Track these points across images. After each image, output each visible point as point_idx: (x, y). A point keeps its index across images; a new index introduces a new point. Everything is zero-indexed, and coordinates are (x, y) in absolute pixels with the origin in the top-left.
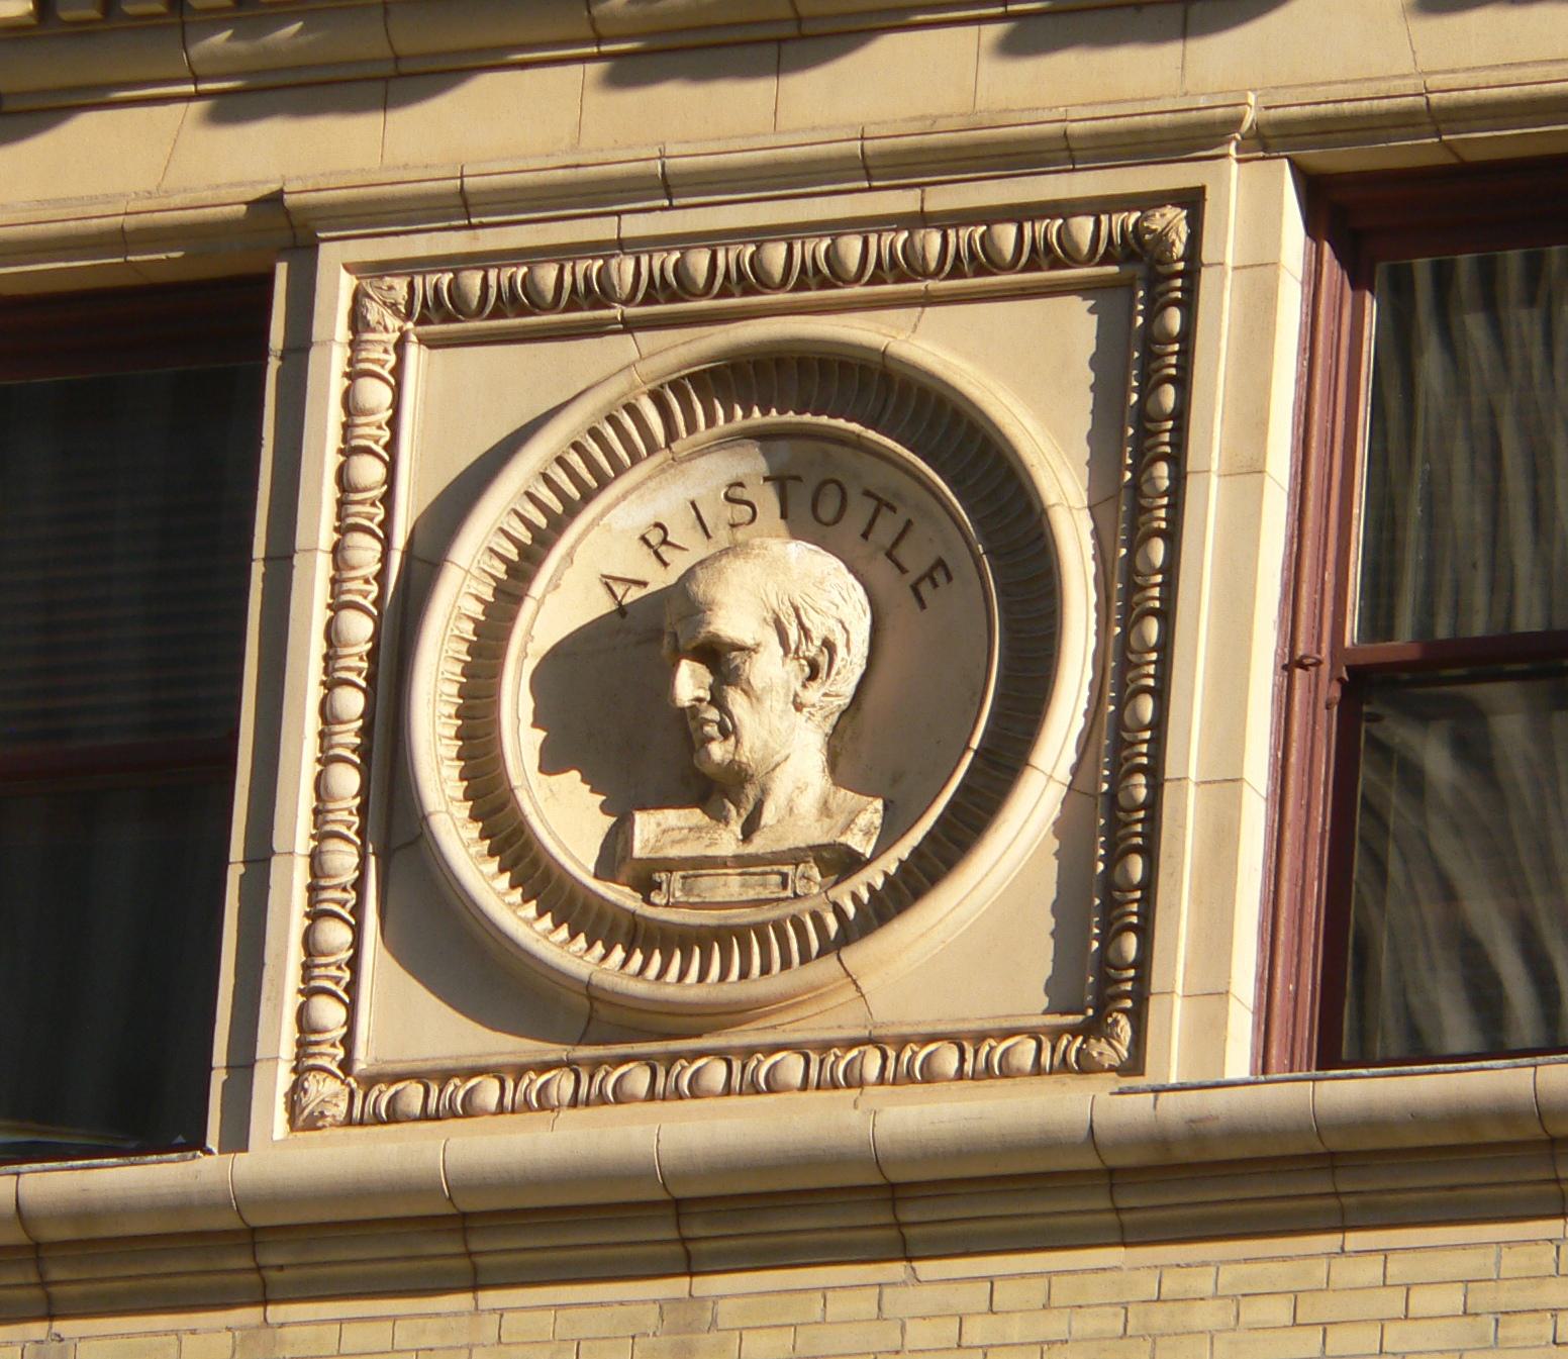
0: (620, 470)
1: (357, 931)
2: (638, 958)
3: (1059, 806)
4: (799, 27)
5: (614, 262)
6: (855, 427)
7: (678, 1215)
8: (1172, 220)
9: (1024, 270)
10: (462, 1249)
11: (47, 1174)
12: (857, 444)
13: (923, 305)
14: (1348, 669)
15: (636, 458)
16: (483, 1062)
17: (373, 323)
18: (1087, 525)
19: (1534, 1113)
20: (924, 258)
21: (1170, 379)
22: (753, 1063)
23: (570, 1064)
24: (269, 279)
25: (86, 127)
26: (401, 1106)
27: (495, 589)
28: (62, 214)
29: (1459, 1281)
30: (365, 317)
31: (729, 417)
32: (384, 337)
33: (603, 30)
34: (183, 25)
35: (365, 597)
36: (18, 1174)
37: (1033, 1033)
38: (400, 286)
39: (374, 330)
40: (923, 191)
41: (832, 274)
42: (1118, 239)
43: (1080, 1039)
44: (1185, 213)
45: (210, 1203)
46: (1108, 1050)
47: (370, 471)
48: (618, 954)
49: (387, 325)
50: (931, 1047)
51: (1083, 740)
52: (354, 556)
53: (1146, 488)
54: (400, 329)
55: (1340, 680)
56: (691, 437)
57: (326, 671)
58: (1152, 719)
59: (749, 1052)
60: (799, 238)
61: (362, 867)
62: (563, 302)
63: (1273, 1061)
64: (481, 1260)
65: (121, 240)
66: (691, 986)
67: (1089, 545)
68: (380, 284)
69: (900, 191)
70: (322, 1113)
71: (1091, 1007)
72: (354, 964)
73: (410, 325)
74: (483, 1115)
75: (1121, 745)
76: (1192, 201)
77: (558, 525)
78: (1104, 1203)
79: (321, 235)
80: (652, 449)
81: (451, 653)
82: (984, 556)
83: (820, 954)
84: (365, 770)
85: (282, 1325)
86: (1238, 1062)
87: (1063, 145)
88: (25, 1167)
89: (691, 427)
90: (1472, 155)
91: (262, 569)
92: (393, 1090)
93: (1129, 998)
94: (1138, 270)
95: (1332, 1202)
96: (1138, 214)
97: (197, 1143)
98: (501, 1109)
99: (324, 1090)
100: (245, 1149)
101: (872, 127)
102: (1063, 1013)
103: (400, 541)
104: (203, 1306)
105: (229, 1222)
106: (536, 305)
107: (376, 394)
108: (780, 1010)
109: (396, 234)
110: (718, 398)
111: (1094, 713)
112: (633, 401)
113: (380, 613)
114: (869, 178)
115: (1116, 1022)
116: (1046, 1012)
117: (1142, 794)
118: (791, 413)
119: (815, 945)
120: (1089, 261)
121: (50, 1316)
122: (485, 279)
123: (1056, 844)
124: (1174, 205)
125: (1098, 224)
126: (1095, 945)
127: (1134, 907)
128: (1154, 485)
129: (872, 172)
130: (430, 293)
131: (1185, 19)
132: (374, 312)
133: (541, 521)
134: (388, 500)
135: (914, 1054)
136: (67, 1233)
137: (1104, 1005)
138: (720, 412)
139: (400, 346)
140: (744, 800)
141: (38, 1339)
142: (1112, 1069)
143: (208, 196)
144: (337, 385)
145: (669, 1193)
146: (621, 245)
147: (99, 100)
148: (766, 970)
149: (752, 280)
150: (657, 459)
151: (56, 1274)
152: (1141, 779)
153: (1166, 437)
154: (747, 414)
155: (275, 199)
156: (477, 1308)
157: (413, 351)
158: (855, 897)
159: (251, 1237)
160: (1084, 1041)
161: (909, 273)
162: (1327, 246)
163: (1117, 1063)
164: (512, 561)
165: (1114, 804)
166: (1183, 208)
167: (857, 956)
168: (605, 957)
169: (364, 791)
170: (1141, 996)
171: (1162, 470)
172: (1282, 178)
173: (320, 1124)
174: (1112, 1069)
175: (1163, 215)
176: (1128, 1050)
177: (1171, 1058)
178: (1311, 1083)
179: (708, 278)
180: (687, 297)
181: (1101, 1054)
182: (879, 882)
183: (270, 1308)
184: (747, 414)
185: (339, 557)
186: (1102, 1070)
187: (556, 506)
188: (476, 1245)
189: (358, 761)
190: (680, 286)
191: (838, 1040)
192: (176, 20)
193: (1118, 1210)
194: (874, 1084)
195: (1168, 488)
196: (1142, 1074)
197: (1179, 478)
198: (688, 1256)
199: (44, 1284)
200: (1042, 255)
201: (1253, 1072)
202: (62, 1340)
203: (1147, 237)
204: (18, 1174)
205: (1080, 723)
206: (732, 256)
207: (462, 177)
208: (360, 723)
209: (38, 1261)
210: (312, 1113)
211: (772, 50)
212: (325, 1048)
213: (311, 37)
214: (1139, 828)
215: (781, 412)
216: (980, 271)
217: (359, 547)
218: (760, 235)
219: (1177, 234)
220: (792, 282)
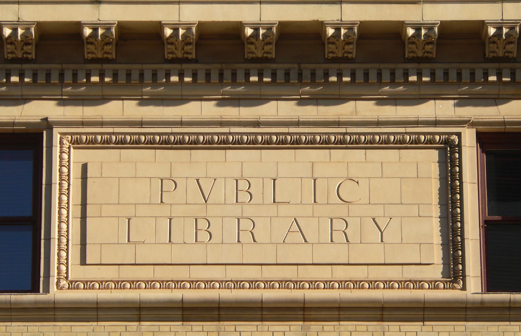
9: (102, 144)
10: (139, 313)
16: (423, 279)
17: (64, 144)
19: (382, 302)
20: (406, 140)
24: (43, 133)
29: (152, 331)
30: (63, 142)
32: (66, 146)
34: (142, 85)
37: (441, 281)
39: (65, 145)
40: (289, 129)
42: (444, 140)
44: (457, 136)
45: (44, 302)
46: (458, 286)
52: (63, 185)
54: (69, 145)
57: (59, 206)
58: (460, 226)
68: (65, 136)
70: (64, 287)
71: (452, 277)
73: (71, 145)
74: (245, 289)
76: (459, 135)
79: (54, 126)
85: (142, 325)
91: (45, 186)
93: (461, 276)
97: (38, 291)
99: (63, 283)
100: (49, 293)
101: (17, 117)
102: (446, 278)
104: (411, 321)
105: (337, 306)
106: (242, 143)
107: (65, 156)
109: (185, 127)
114: (83, 126)
115: (460, 281)
116: (442, 278)
127: (460, 260)
130: (76, 139)
132: (65, 141)
139: (69, 148)
142: (459, 289)
144: (58, 154)
147: (40, 98)
152: (459, 238)
155: (46, 119)
157: (72, 149)
163: (460, 288)
166: (457, 136)
173: (63, 289)
174: (459, 289)
175: (453, 137)
176: (462, 286)
186: (457, 289)
188: (341, 313)
198: (219, 318)
200: (414, 142)
203: (450, 140)
207: (142, 118)
209: (424, 310)
210: (62, 287)
212: (63, 274)
214: (460, 246)
218: (360, 134)
219: (456, 140)
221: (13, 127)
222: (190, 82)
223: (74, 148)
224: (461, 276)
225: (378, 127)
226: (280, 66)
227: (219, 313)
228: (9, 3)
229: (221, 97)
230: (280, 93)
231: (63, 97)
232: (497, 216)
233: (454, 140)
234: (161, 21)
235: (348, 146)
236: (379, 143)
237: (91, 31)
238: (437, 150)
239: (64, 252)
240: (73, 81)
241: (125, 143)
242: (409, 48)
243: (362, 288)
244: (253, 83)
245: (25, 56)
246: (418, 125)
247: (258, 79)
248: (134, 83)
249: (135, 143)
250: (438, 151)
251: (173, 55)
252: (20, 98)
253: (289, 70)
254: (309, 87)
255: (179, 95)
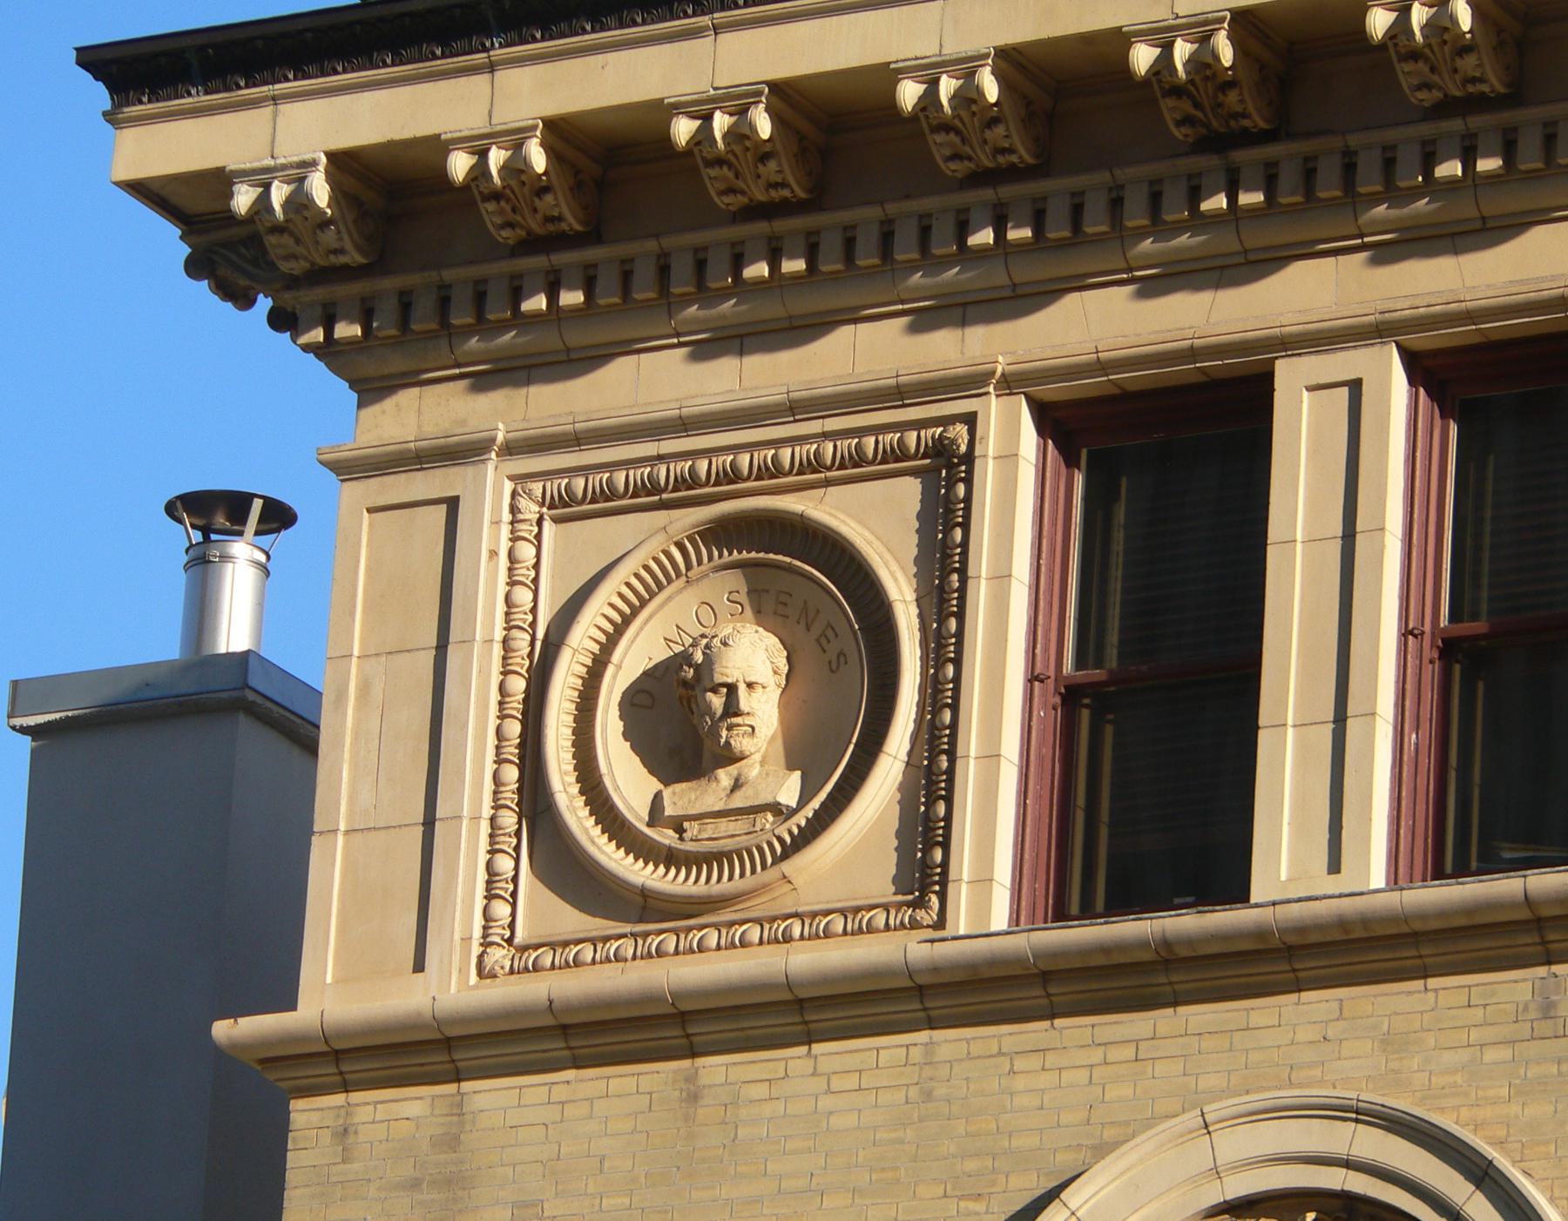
0: (660, 587)
1: (517, 860)
2: (673, 871)
3: (901, 775)
4: (568, 355)
5: (656, 468)
6: (788, 560)
7: (684, 1021)
8: (960, 431)
9: (880, 464)
11: (1544, 876)
12: (790, 569)
13: (826, 487)
14: (1065, 687)
15: (670, 581)
18: (914, 611)
21: (959, 524)
22: (776, 925)
23: (635, 935)
25: (843, 335)
26: (874, 924)
27: (593, 659)
28: (1525, 289)
31: (721, 556)
33: (1133, 264)
34: (1354, 203)
35: (522, 668)
36: (1525, 876)
37: (886, 907)
38: (537, 488)
41: (773, 470)
43: (911, 909)
44: (966, 427)
46: (927, 917)
47: (523, 596)
48: (662, 869)
49: (530, 509)
50: (745, 927)
51: (914, 737)
53: (947, 588)
54: (539, 512)
55: (1060, 694)
56: (700, 568)
59: (731, 924)
60: (550, 479)
61: (520, 823)
62: (670, 487)
63: (1023, 919)
64: (347, 1077)
65: (1192, 354)
66: (713, 885)
67: (916, 622)
69: (894, 410)
71: (917, 891)
72: (515, 879)
73: (545, 510)
74: (665, 956)
75: (933, 739)
76: (970, 420)
77: (627, 621)
78: (333, 1070)
80: (678, 575)
81: (568, 697)
82: (858, 632)
83: (772, 864)
84: (521, 768)
86: (1000, 919)
87: (896, 391)
88: (1529, 872)
89: (700, 563)
90: (1494, 337)
92: (534, 955)
94: (942, 461)
95: (1418, 962)
96: (942, 429)
98: (845, 933)
99: (499, 956)
102: (904, 894)
103: (540, 634)
104: (1163, 1004)
108: (749, 899)
110: (714, 545)
111: (919, 721)
112: (667, 548)
113: (530, 676)
116: (895, 894)
117: (945, 765)
118: (754, 553)
119: (769, 860)
120: (915, 457)
121: (1549, 963)
122: (627, 477)
123: (898, 796)
124: (960, 423)
125: (710, 464)
126: (919, 855)
128: (950, 587)
129: (1011, 384)
131: (964, 315)
132: (523, 503)
133: (618, 619)
134: (534, 610)
135: (779, 926)
136: (1557, 911)
137: (924, 890)
138: (716, 553)
140: (707, 778)
141: (1542, 976)
142: (928, 926)
143: (1133, 341)
145: (677, 1008)
146: (660, 458)
148: (742, 875)
149: (733, 475)
150: (684, 579)
151: (1551, 937)
152: (944, 757)
153: (957, 558)
154: (730, 554)
156: (1426, 989)
158: (790, 832)
159: (682, 1017)
160: (913, 911)
161: (652, 490)
162: (1422, 390)
163: (931, 923)
164: (603, 643)
165: (930, 772)
166: (965, 424)
167: (787, 867)
168: (654, 871)
169: (520, 780)
170: (944, 882)
171: (955, 577)
172: (1391, 357)
174: (928, 926)
176: (938, 915)
177: (961, 922)
178: (1149, 921)
179: (874, 454)
180: (905, 459)
181: (921, 918)
182: (803, 823)
183: (462, 1084)
184: (730, 554)
185: (506, 645)
187: (627, 610)
188: (345, 1068)
189: (517, 761)
190: (692, 481)
191: (865, 906)
192: (446, 332)
193: (570, 1048)
194: (798, 940)
195: (958, 587)
196: (944, 929)
197: (964, 580)
199: (1544, 943)
201: (1009, 926)
202: (1556, 977)
204: (1525, 876)
205: (911, 726)
206: (555, 487)
208: (518, 740)
209: (1540, 930)
211: (737, 341)
213: (969, 275)
215: (748, 552)
216: (856, 465)
217: (516, 639)
218: (861, 432)
219: (962, 439)
220: (753, 477)
221: (1195, 363)
222: (1496, 173)
223: (557, 520)
224: (936, 883)
225: (688, 436)
226: (1131, 172)
227: (1047, 992)
228: (474, 70)
229: (900, 307)
230: (1081, 270)
231: (1366, 240)
232: (1098, 671)
233: (956, 440)
234: (440, 135)
235: (829, 474)
236: (920, 455)
237: (1392, 16)
238: (916, 478)
239: (507, 856)
240: (1113, 227)
241: (781, 473)
242: (1407, 75)
243: (615, 958)
244: (1212, 217)
245: (1001, 159)
246: (579, 446)
247: (783, 264)
248: (831, 273)
249: (890, 459)
250: (920, 480)
251: (1430, 91)
252: (564, 358)
253: (1045, 199)
254: (1386, 205)
255: (1003, 287)
